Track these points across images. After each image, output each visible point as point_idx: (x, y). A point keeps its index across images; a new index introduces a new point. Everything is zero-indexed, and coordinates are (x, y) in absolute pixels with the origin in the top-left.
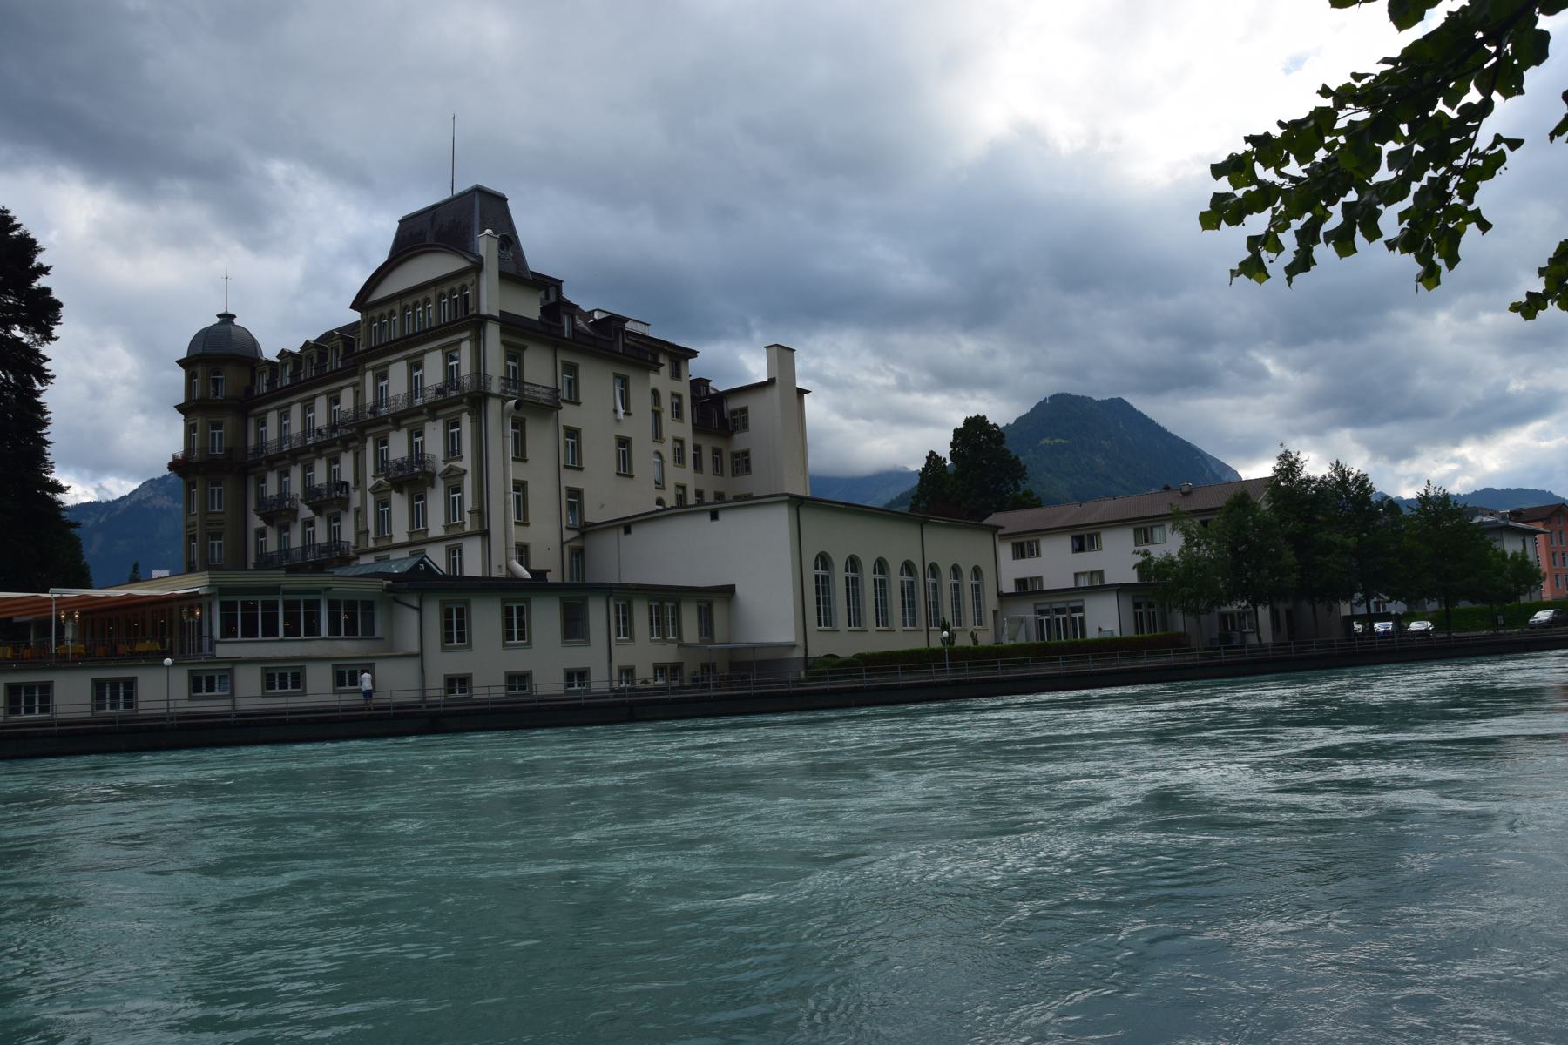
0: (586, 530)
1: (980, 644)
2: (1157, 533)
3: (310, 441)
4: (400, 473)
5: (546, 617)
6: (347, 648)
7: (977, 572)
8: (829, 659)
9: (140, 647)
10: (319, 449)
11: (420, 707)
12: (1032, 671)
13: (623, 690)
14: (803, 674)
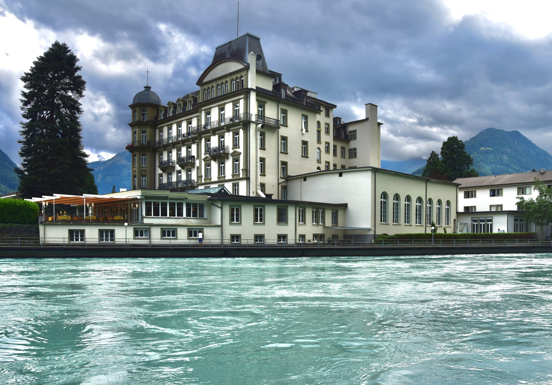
0: (288, 179)
1: (447, 233)
2: (528, 190)
3: (180, 139)
4: (215, 153)
5: (271, 213)
6: (193, 222)
7: (448, 203)
8: (384, 236)
9: (116, 218)
10: (183, 143)
11: (221, 246)
12: (469, 245)
13: (300, 244)
14: (373, 241)
